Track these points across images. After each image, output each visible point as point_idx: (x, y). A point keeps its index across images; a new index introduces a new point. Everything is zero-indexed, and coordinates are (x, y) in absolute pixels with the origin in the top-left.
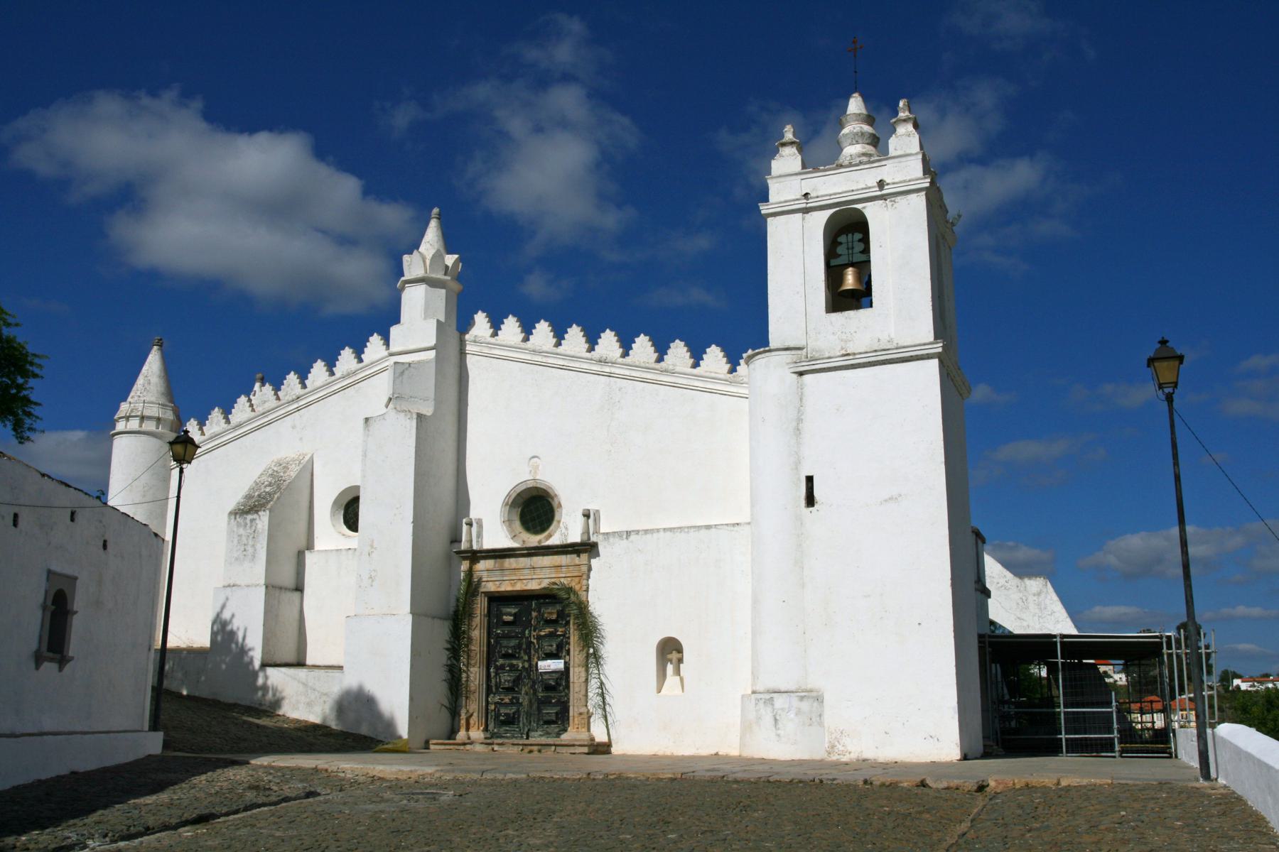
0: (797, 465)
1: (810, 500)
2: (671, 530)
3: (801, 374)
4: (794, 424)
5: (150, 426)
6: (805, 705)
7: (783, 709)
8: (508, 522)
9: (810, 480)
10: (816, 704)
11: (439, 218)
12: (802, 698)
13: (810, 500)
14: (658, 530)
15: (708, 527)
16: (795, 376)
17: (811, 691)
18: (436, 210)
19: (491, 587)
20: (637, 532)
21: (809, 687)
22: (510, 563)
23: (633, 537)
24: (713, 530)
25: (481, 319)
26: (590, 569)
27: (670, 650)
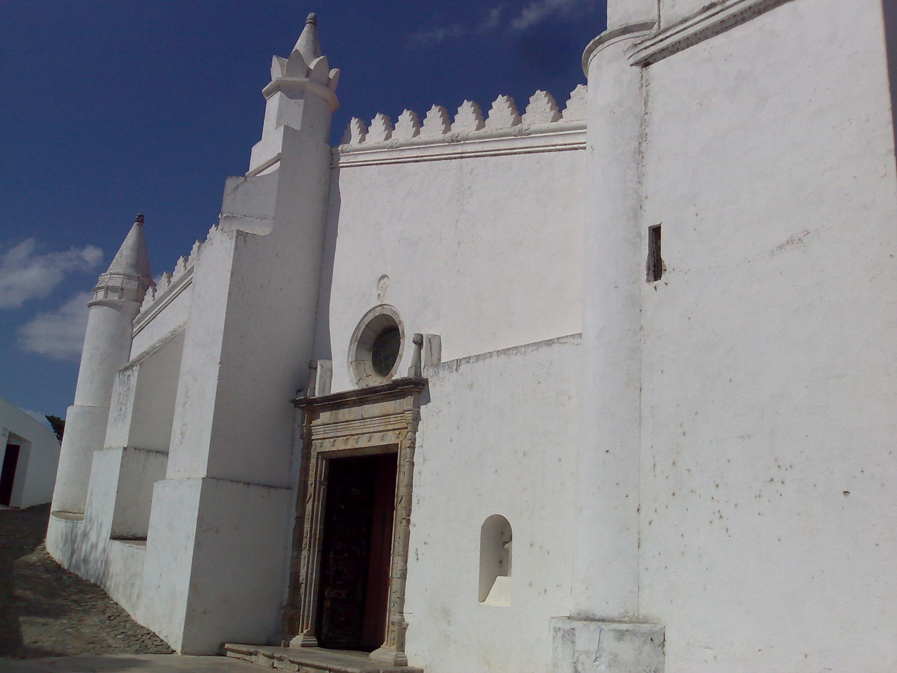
0: (638, 209)
1: (656, 269)
2: (506, 351)
3: (646, 63)
4: (634, 144)
5: (114, 297)
6: (627, 650)
7: (587, 652)
8: (357, 362)
9: (656, 232)
10: (648, 648)
11: (314, 23)
12: (621, 635)
13: (656, 269)
14: (491, 354)
15: (549, 343)
16: (637, 69)
17: (645, 621)
18: (311, 15)
19: (328, 446)
20: (468, 359)
21: (643, 612)
22: (345, 414)
23: (464, 367)
24: (555, 346)
25: (354, 125)
26: (417, 418)
27: (498, 538)
